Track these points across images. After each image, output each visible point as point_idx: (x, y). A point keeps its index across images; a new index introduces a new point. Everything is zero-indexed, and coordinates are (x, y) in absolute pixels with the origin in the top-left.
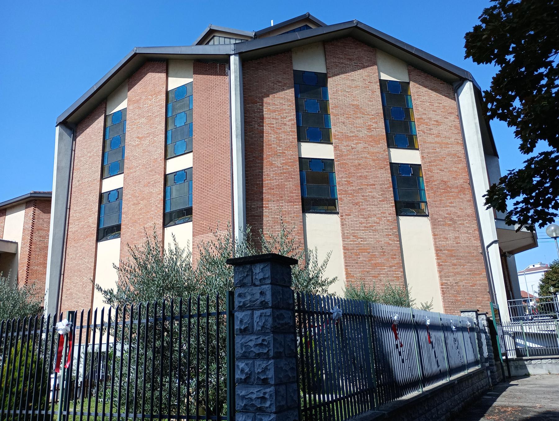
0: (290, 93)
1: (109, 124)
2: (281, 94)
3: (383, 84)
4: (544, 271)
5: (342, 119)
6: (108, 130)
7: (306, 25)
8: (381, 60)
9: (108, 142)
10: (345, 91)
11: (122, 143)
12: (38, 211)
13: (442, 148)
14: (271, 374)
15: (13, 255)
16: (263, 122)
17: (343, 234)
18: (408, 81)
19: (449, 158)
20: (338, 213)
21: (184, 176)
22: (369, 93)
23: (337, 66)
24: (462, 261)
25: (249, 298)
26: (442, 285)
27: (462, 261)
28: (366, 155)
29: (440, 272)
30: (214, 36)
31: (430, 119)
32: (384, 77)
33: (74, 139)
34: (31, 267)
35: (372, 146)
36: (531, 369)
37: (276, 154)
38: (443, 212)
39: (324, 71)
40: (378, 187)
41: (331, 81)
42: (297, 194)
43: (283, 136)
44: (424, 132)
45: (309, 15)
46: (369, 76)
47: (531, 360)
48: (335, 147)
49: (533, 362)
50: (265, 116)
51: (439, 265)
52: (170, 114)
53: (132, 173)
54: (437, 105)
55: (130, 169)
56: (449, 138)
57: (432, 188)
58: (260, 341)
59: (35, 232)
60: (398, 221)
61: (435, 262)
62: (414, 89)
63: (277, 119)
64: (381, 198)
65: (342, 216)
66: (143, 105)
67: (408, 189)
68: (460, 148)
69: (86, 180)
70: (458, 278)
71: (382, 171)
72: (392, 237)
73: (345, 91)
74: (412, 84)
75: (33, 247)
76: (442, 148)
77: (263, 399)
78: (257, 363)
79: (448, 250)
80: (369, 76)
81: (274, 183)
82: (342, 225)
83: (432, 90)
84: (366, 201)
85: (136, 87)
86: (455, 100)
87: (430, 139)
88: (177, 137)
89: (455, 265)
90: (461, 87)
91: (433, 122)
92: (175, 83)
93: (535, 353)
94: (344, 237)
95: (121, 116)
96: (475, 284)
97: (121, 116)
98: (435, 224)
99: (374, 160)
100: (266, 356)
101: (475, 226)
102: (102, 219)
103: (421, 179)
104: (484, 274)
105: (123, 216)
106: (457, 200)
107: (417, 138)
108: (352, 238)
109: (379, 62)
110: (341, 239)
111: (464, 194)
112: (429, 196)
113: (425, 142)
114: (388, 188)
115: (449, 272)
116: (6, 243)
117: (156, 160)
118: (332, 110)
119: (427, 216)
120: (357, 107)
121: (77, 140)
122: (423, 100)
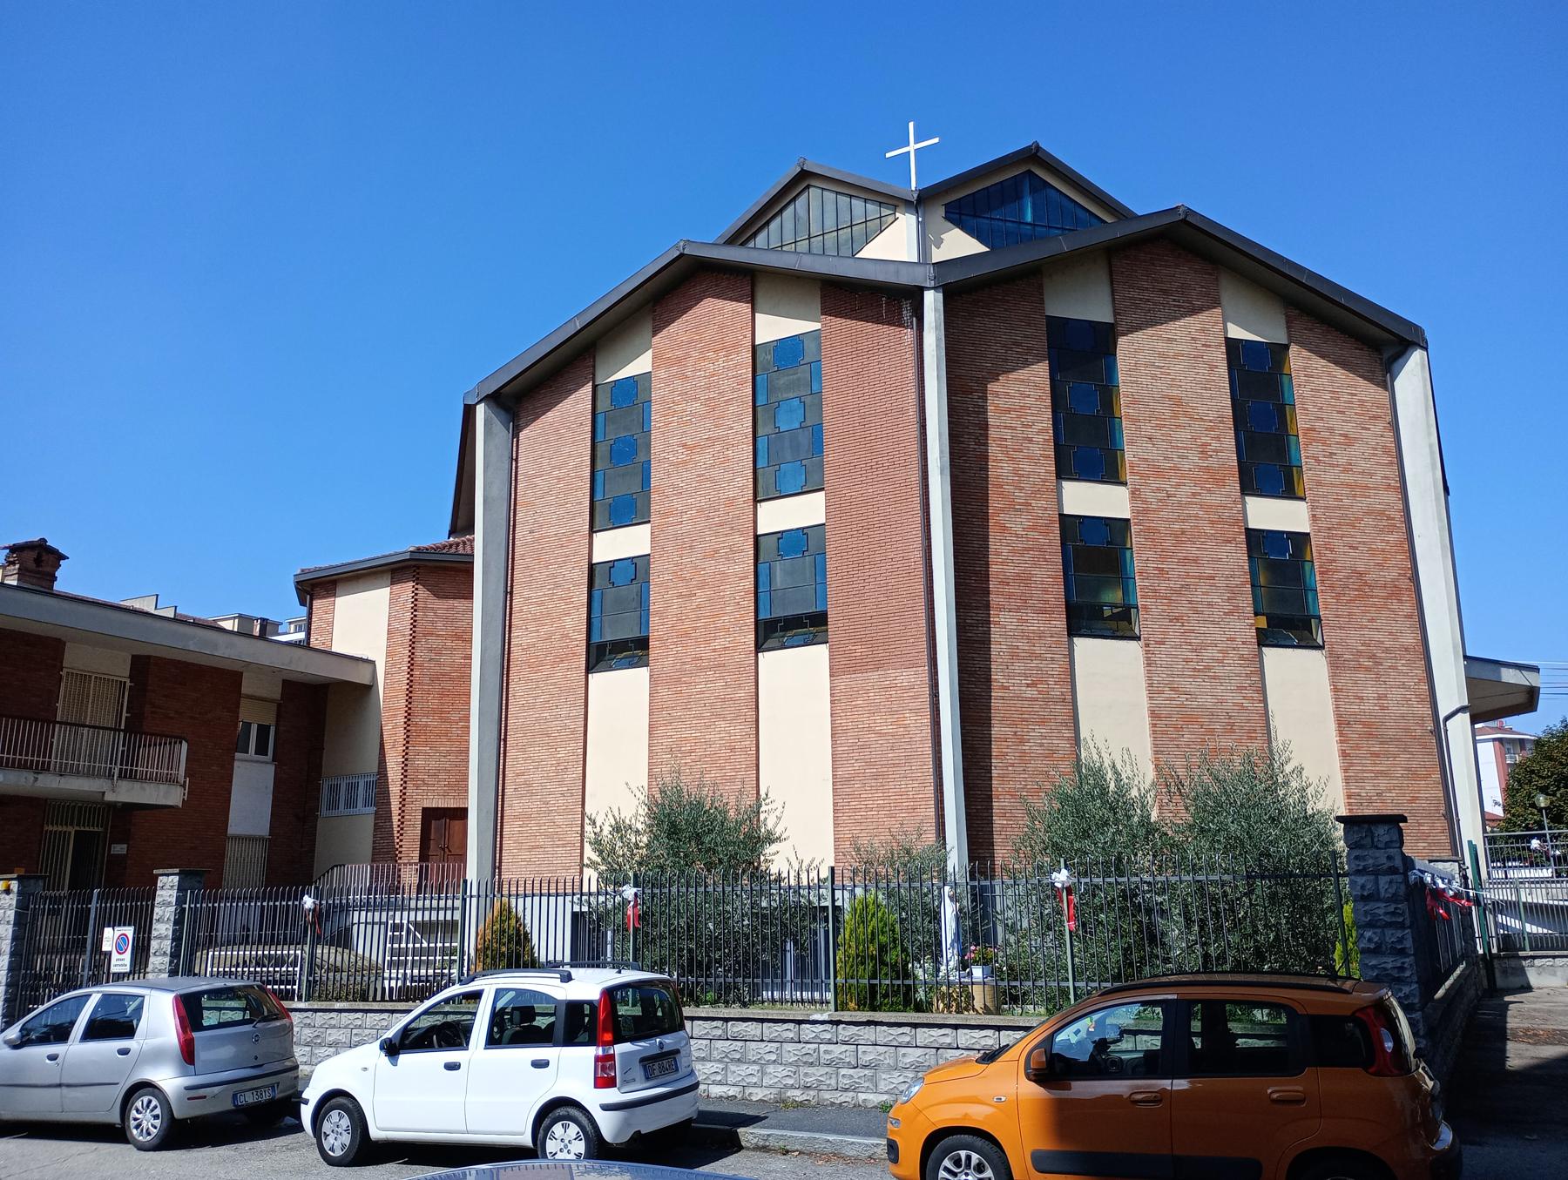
0: (1039, 373)
1: (603, 404)
2: (1023, 374)
3: (1232, 346)
4: (1494, 740)
5: (1147, 429)
6: (600, 419)
7: (1029, 171)
8: (1230, 293)
9: (602, 449)
10: (1153, 365)
11: (641, 458)
12: (423, 593)
13: (1355, 496)
14: (1408, 943)
15: (365, 691)
16: (987, 438)
17: (1151, 685)
18: (1285, 342)
19: (1369, 521)
20: (1139, 638)
21: (800, 542)
22: (1203, 370)
23: (1137, 307)
24: (1392, 749)
25: (1371, 861)
26: (1349, 797)
27: (1392, 749)
28: (1194, 511)
29: (1346, 771)
30: (808, 187)
31: (1331, 430)
32: (1236, 332)
33: (516, 435)
34: (415, 720)
35: (1209, 491)
36: (1533, 978)
37: (1012, 507)
38: (1354, 639)
39: (1109, 319)
40: (1221, 583)
41: (1126, 346)
42: (1056, 595)
43: (1027, 467)
44: (1317, 460)
45: (1038, 148)
46: (1203, 330)
47: (1534, 957)
48: (1133, 493)
49: (1537, 962)
50: (991, 421)
51: (1344, 754)
52: (761, 400)
53: (672, 524)
54: (1346, 398)
55: (666, 515)
56: (1371, 475)
57: (1332, 587)
58: (1391, 909)
59: (414, 639)
60: (1260, 656)
61: (1335, 748)
62: (1298, 358)
63: (1014, 429)
64: (1227, 607)
65: (1147, 645)
66: (694, 371)
67: (1284, 593)
68: (1393, 498)
69: (552, 531)
70: (1383, 783)
71: (1229, 547)
72: (1249, 693)
73: (1153, 365)
74: (1294, 349)
75: (416, 673)
76: (1355, 496)
77: (1402, 969)
78: (1389, 932)
79: (1364, 724)
80: (1203, 330)
81: (1011, 570)
82: (1149, 665)
83: (1336, 363)
84: (1197, 612)
85: (673, 328)
86: (1386, 388)
87: (1330, 476)
88: (785, 456)
89: (1377, 755)
90: (1401, 360)
91: (1338, 439)
92: (773, 327)
93: (1539, 943)
94: (1153, 691)
95: (635, 393)
96: (1417, 798)
97: (635, 393)
98: (1336, 665)
99: (1212, 522)
100: (1402, 926)
101: (1421, 673)
102: (595, 622)
103: (1307, 566)
104: (1437, 776)
105: (654, 620)
106: (1385, 613)
107: (1301, 473)
108: (1168, 693)
109: (1226, 297)
110: (1145, 693)
111: (1400, 601)
112: (1325, 604)
113: (1319, 483)
114: (1243, 585)
115: (1364, 771)
116: (353, 663)
117: (731, 502)
118: (1124, 407)
119: (1321, 648)
120: (1178, 402)
121: (522, 435)
122: (1317, 384)
